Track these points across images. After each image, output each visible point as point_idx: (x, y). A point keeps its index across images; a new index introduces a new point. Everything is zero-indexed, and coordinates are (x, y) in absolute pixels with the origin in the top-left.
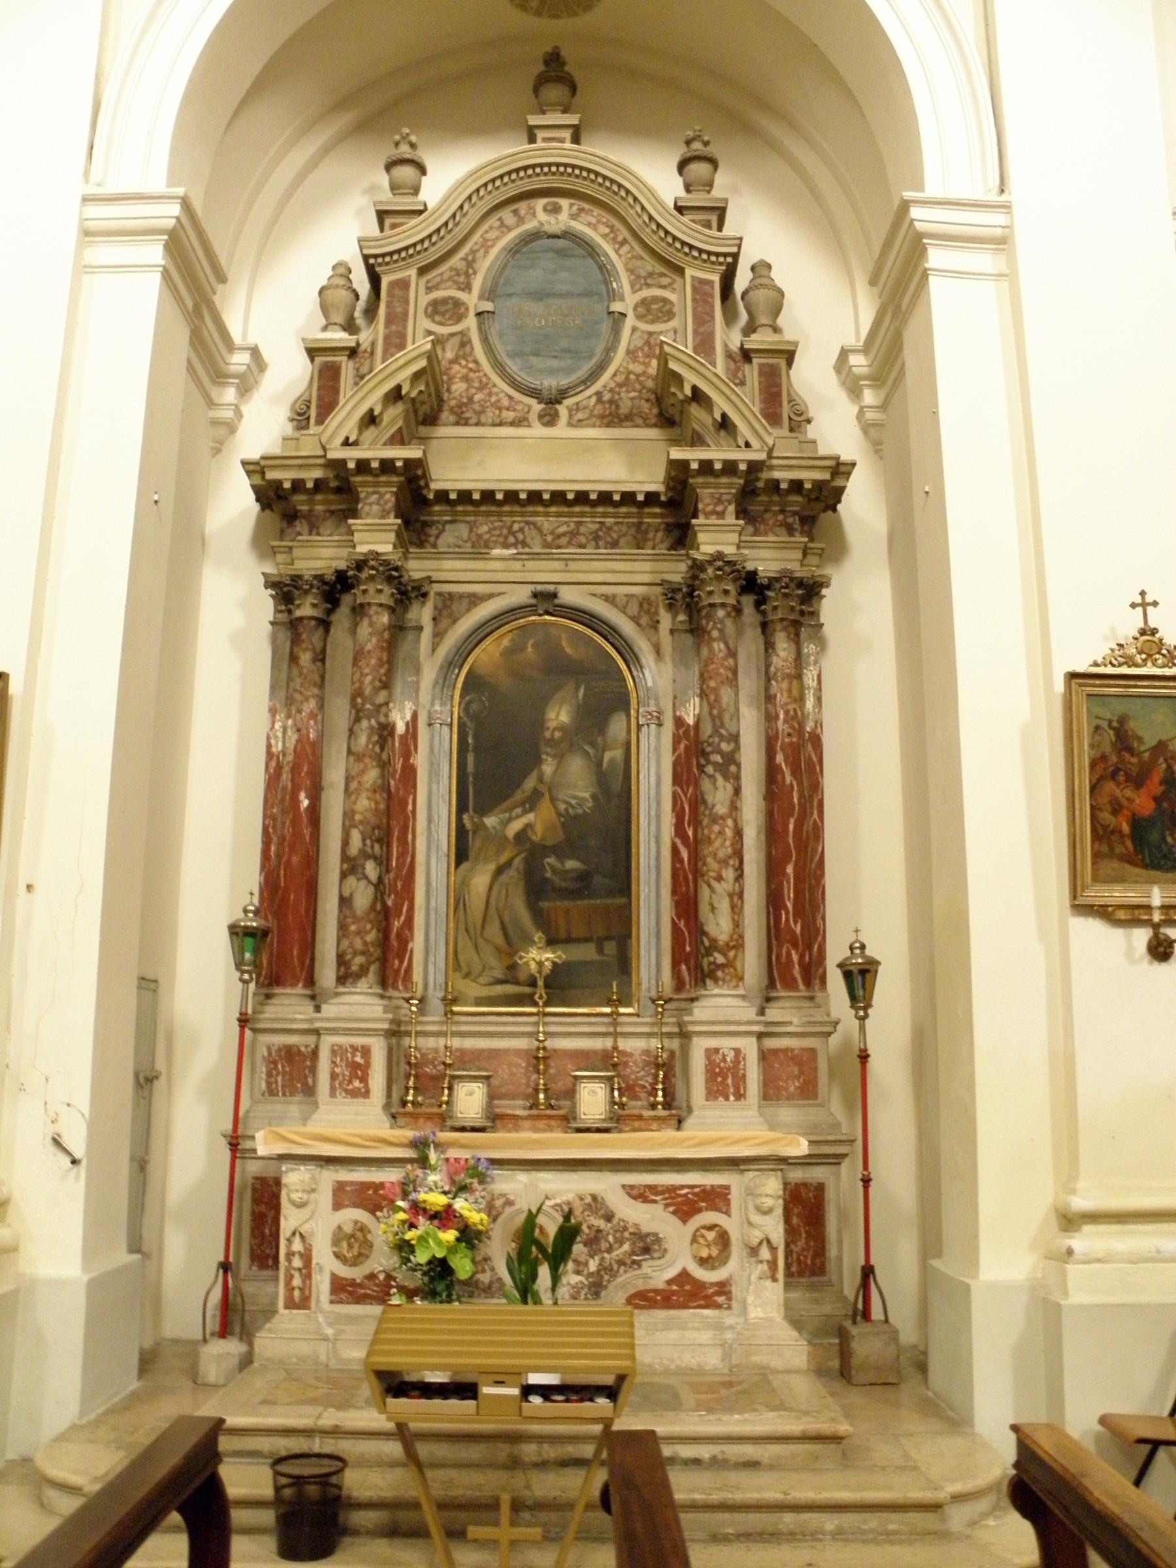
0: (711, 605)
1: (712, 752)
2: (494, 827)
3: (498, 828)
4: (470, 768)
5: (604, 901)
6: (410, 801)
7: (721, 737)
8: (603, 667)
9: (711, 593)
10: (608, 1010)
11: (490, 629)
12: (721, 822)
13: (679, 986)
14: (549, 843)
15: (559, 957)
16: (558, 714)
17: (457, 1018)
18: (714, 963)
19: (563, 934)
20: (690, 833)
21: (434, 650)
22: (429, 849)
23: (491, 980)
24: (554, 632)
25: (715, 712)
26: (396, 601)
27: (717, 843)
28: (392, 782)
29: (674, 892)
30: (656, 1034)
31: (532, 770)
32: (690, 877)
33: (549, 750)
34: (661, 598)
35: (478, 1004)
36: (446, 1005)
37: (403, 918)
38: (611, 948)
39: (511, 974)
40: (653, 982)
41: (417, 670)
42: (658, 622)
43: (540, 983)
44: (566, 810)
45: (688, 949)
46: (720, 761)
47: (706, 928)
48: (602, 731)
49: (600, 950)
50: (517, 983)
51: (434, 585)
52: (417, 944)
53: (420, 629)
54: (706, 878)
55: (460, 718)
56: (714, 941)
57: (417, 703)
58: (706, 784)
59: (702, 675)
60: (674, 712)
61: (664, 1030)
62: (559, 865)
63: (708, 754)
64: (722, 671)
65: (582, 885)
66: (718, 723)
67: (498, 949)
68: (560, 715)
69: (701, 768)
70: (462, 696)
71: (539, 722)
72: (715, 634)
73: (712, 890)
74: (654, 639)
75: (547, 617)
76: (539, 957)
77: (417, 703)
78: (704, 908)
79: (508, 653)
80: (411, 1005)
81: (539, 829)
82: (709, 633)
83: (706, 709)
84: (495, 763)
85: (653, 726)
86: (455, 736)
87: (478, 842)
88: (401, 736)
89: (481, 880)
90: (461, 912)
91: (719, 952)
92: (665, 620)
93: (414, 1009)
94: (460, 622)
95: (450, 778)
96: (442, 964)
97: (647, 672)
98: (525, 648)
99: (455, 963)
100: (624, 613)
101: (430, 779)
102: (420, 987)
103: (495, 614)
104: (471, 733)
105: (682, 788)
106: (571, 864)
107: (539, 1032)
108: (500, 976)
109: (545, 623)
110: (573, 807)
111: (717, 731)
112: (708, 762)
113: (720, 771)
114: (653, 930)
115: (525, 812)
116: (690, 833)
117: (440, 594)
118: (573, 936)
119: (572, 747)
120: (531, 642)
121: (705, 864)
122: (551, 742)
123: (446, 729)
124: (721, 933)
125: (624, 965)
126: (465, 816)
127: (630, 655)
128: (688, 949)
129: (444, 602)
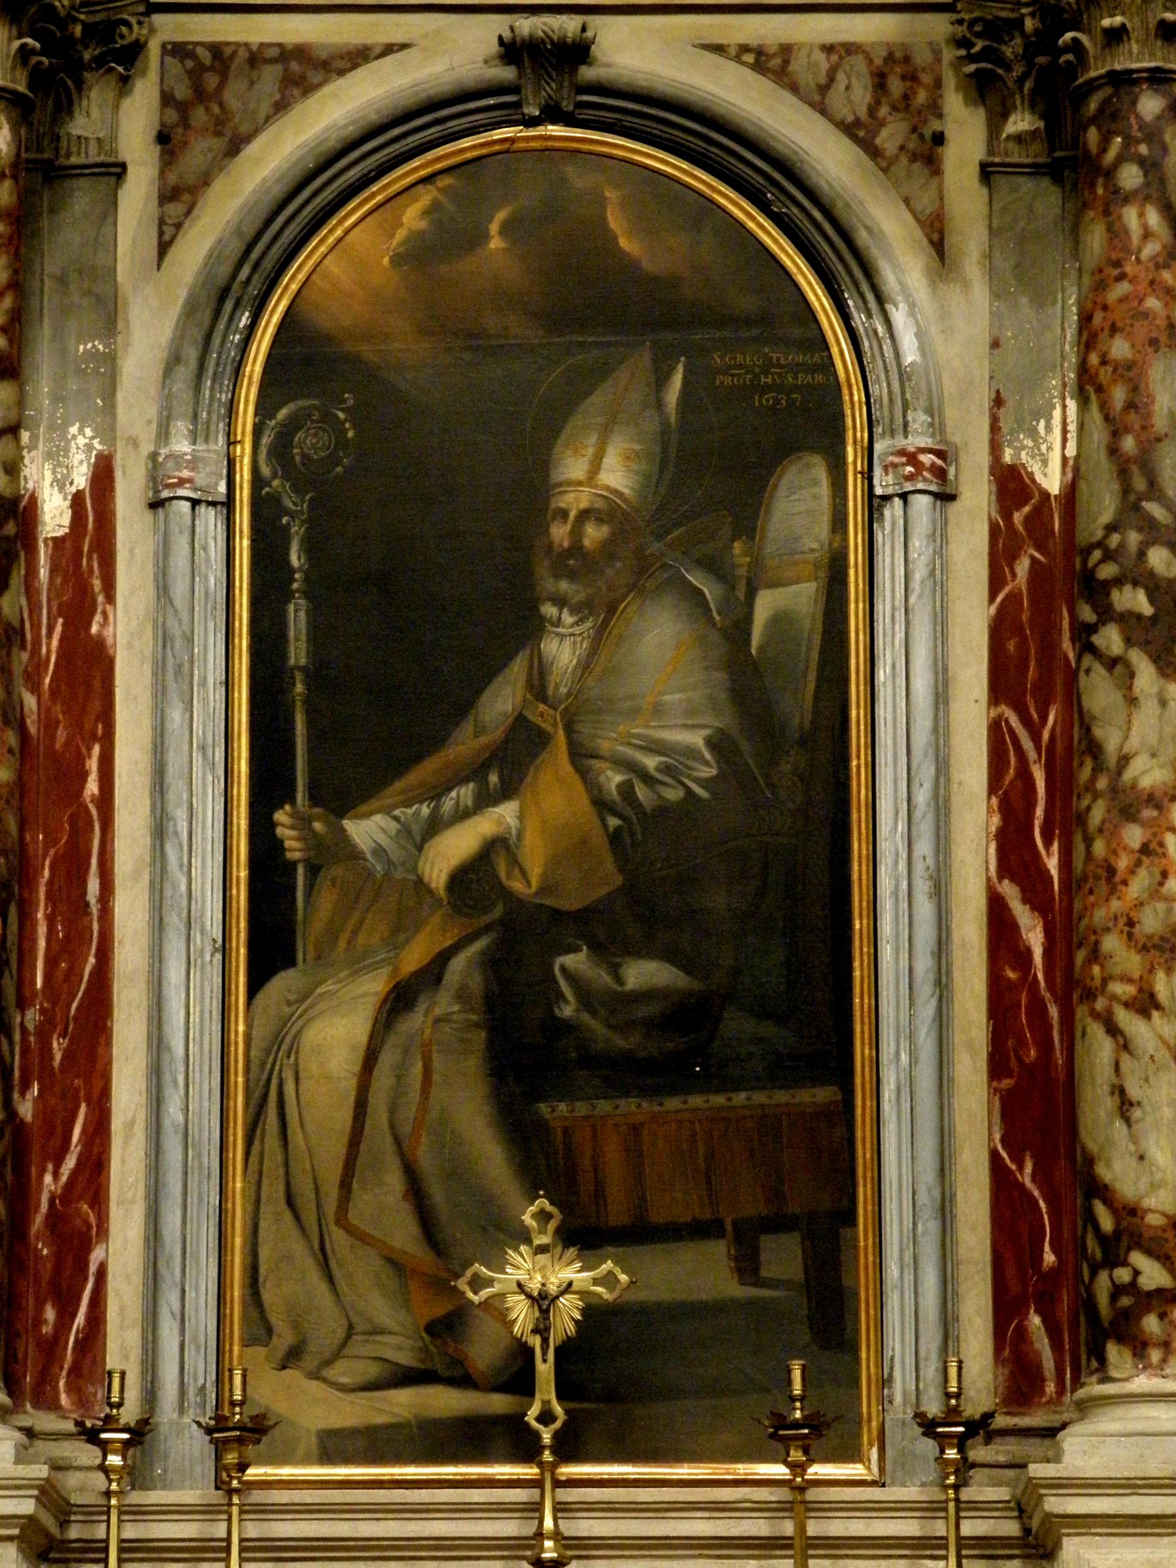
0: (1123, 81)
1: (1119, 581)
2: (379, 851)
3: (396, 855)
4: (298, 652)
5: (759, 1098)
6: (93, 764)
7: (1150, 527)
8: (747, 303)
9: (1116, 36)
10: (778, 1470)
11: (353, 174)
12: (1148, 813)
13: (1021, 1381)
14: (570, 903)
15: (608, 1280)
16: (596, 466)
17: (257, 1496)
18: (1132, 1287)
19: (617, 1213)
20: (1052, 863)
21: (163, 248)
22: (158, 926)
23: (373, 1371)
24: (579, 179)
25: (1129, 443)
26: (37, 78)
27: (1138, 886)
28: (30, 701)
29: (997, 1066)
30: (940, 1543)
31: (509, 658)
32: (1054, 1012)
33: (564, 586)
34: (949, 54)
35: (327, 1457)
36: (220, 1448)
37: (70, 1163)
38: (783, 1258)
39: (443, 1350)
40: (931, 1370)
41: (109, 315)
42: (939, 139)
43: (545, 1370)
44: (626, 790)
45: (1049, 1258)
46: (1147, 609)
47: (1103, 1172)
48: (747, 514)
49: (747, 1266)
50: (463, 1380)
51: (158, 19)
52: (121, 1250)
53: (117, 171)
54: (1100, 1004)
55: (257, 480)
56: (1129, 1212)
57: (108, 429)
58: (1099, 691)
59: (1085, 319)
60: (995, 449)
61: (968, 1528)
62: (603, 978)
63: (1107, 586)
64: (1153, 303)
65: (679, 1047)
66: (1140, 484)
67: (395, 1264)
68: (601, 468)
69: (1084, 634)
70: (264, 409)
71: (534, 491)
72: (1130, 177)
73: (1125, 1045)
74: (925, 202)
75: (554, 130)
76: (538, 1282)
77: (108, 429)
78: (1095, 1105)
79: (418, 257)
80: (105, 1446)
81: (535, 858)
82: (1109, 174)
83: (1099, 434)
84: (378, 642)
85: (921, 503)
86: (243, 544)
87: (327, 900)
88: (58, 542)
89: (336, 1033)
90: (272, 1141)
91: (1150, 1253)
92: (966, 134)
93: (115, 1460)
94: (253, 149)
95: (228, 684)
96: (204, 1319)
97: (899, 316)
98: (478, 238)
99: (252, 1314)
100: (822, 110)
101: (160, 693)
102: (133, 1396)
103: (374, 118)
104: (297, 531)
105: (1026, 720)
106: (644, 973)
107: (540, 1535)
108: (405, 1358)
109: (550, 152)
110: (647, 779)
111: (1137, 508)
112: (1106, 613)
113: (1145, 645)
114: (928, 1198)
115: (485, 800)
116: (1052, 863)
117: (177, 50)
118: (658, 1216)
119: (645, 578)
120: (501, 216)
121: (1095, 955)
122: (573, 562)
123: (210, 519)
124: (1154, 1186)
125: (831, 1315)
126: (281, 816)
127: (845, 261)
128: (1049, 1258)
129: (196, 75)
